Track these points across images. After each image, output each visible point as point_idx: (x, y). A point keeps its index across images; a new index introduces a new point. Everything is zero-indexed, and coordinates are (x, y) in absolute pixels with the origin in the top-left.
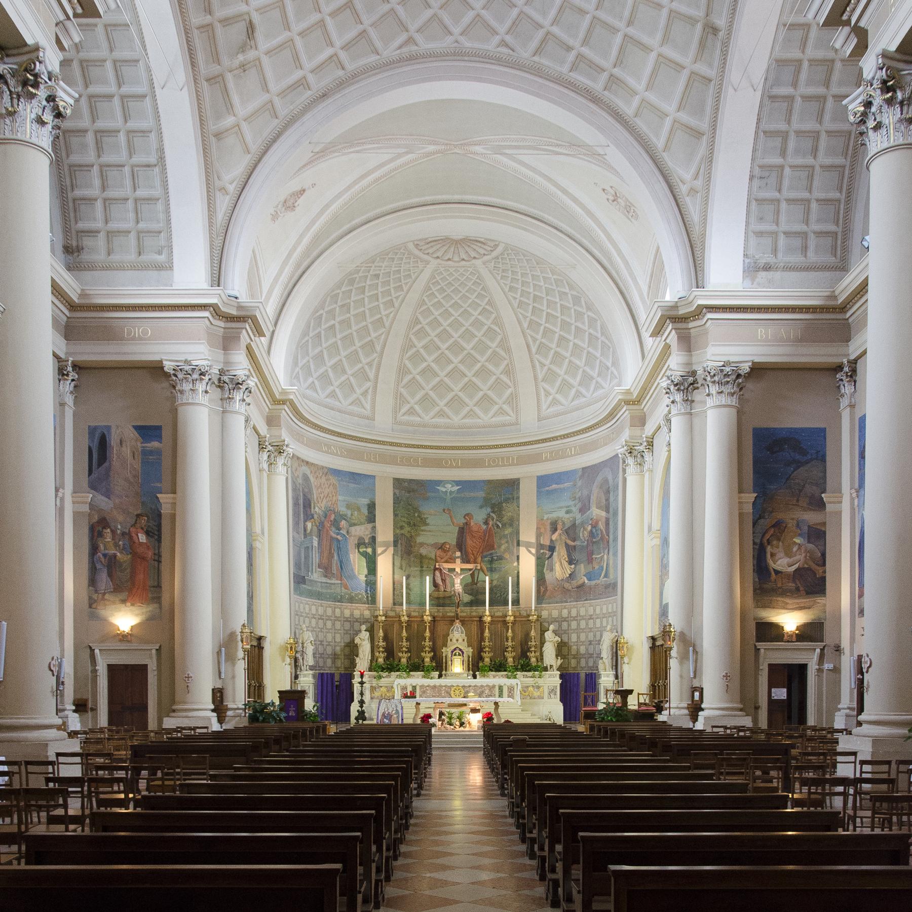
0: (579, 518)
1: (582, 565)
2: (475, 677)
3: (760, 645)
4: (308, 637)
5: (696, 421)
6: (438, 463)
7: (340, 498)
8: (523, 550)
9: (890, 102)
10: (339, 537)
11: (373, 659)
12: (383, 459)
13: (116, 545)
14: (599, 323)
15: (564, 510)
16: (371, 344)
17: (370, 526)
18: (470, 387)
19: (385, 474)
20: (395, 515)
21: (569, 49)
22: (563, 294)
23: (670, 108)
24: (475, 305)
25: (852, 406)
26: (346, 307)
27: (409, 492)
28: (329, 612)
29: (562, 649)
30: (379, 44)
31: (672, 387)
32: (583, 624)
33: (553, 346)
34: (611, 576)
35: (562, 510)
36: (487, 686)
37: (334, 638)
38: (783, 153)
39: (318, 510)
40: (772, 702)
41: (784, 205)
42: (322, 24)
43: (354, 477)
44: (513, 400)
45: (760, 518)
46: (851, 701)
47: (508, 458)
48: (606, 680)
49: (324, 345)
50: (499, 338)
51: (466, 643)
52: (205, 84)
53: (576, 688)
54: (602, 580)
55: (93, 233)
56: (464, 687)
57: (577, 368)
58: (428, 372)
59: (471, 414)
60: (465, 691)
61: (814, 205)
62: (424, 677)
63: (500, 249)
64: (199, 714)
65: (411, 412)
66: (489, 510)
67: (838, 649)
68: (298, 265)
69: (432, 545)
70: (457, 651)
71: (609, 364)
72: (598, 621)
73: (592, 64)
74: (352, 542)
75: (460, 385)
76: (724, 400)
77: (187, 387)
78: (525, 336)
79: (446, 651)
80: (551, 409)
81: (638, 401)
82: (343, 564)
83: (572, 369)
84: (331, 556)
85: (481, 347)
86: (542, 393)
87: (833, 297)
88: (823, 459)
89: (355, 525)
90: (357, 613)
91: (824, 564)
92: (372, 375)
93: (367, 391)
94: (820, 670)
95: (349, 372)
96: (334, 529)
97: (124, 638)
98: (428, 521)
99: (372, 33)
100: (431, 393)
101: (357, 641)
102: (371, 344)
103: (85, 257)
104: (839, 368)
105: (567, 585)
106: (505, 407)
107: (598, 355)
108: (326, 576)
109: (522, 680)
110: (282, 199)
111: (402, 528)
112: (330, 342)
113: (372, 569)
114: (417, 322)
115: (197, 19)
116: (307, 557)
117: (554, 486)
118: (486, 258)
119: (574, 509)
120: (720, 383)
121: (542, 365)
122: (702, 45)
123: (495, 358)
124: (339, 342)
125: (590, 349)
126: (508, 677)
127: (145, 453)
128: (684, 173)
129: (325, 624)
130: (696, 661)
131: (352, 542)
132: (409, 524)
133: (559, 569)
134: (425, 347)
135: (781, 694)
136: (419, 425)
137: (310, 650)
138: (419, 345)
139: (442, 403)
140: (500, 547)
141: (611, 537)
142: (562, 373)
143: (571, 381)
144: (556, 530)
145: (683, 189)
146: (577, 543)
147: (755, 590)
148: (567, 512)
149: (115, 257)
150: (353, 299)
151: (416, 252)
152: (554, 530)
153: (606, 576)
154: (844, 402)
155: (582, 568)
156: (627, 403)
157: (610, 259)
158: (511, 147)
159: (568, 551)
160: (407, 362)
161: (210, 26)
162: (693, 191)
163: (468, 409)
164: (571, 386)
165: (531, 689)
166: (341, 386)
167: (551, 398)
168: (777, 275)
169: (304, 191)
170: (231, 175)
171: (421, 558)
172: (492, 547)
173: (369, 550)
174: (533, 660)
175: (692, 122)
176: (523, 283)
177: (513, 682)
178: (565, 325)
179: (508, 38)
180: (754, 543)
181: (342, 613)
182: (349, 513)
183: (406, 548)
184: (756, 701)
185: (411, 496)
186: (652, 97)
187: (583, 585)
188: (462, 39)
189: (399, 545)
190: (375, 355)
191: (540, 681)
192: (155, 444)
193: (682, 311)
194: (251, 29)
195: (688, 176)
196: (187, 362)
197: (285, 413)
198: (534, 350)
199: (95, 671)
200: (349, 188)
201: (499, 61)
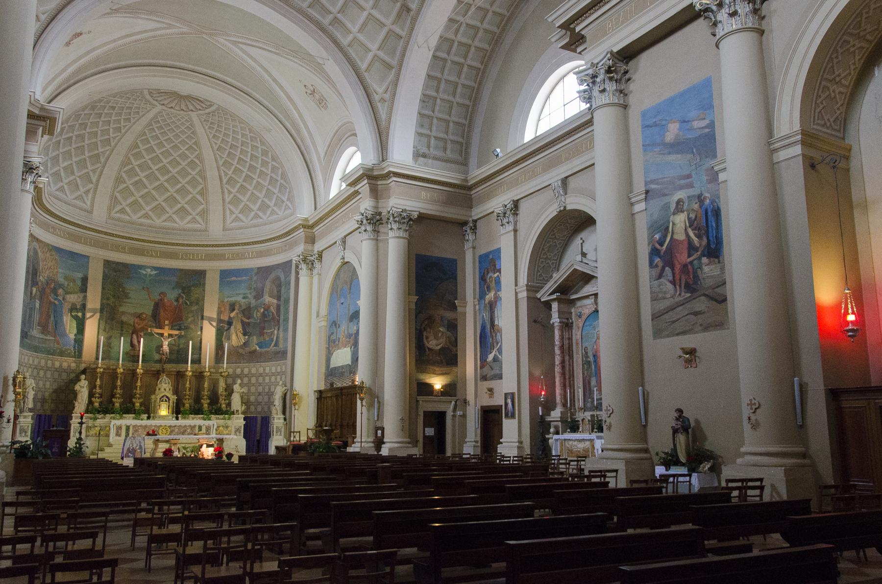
0: (253, 303)
1: (255, 337)
2: (177, 418)
3: (419, 398)
5: (381, 244)
6: (141, 252)
7: (60, 271)
8: (206, 324)
10: (56, 302)
11: (90, 402)
12: (97, 244)
14: (280, 171)
15: (241, 296)
16: (97, 156)
17: (82, 295)
18: (171, 200)
19: (98, 255)
20: (103, 288)
22: (254, 148)
23: (374, 47)
24: (183, 142)
25: (474, 248)
26: (84, 126)
27: (116, 272)
28: (43, 363)
31: (365, 221)
32: (253, 380)
33: (241, 180)
34: (281, 346)
35: (240, 296)
36: (190, 426)
37: (44, 385)
38: (437, 91)
39: (41, 278)
40: (425, 437)
41: (435, 121)
43: (72, 255)
44: (204, 213)
45: (420, 312)
46: (476, 436)
47: (198, 254)
48: (277, 421)
49: (61, 151)
50: (198, 169)
53: (256, 430)
54: (272, 348)
56: (170, 427)
57: (258, 198)
58: (139, 184)
59: (170, 219)
60: (171, 429)
61: (451, 124)
62: (135, 418)
63: (213, 109)
65: (122, 211)
66: (180, 291)
67: (465, 402)
68: (60, 86)
69: (132, 314)
71: (285, 199)
74: (66, 307)
76: (401, 233)
80: (233, 224)
81: (312, 227)
82: (58, 323)
83: (253, 198)
85: (183, 173)
86: (228, 212)
87: (466, 180)
88: (455, 278)
90: (65, 365)
91: (456, 346)
92: (94, 180)
93: (88, 191)
94: (454, 416)
95: (77, 174)
98: (130, 295)
100: (140, 200)
101: (77, 387)
102: (97, 156)
104: (465, 223)
105: (241, 351)
107: (276, 191)
108: (43, 333)
109: (215, 421)
111: (108, 299)
112: (66, 149)
113: (81, 330)
114: (137, 146)
116: (30, 316)
117: (234, 278)
118: (200, 112)
119: (249, 296)
120: (399, 222)
121: (230, 192)
122: (399, 16)
123: (193, 182)
124: (73, 150)
125: (270, 187)
128: (378, 89)
129: (38, 373)
130: (379, 409)
132: (114, 296)
133: (236, 338)
135: (430, 432)
136: (129, 222)
137: (31, 395)
139: (148, 208)
140: (187, 319)
141: (282, 317)
143: (252, 207)
144: (234, 310)
145: (377, 98)
146: (251, 320)
147: (416, 360)
148: (244, 298)
150: (91, 120)
151: (148, 97)
153: (276, 345)
154: (468, 246)
155: (255, 339)
156: (304, 226)
157: (298, 131)
159: (243, 325)
160: (124, 175)
162: (382, 100)
163: (168, 215)
164: (251, 210)
165: (221, 428)
166: (69, 183)
167: (234, 216)
168: (430, 161)
169: (81, 34)
171: (122, 323)
172: (181, 319)
173: (80, 314)
174: (224, 406)
175: (387, 59)
176: (225, 134)
177: (207, 423)
178: (252, 168)
180: (416, 329)
181: (53, 364)
182: (66, 283)
183: (110, 315)
184: (416, 437)
185: (117, 276)
186: (361, 37)
187: (255, 351)
190: (99, 165)
191: (229, 422)
193: (375, 173)
195: (380, 90)
198: (225, 181)
200: (115, 41)
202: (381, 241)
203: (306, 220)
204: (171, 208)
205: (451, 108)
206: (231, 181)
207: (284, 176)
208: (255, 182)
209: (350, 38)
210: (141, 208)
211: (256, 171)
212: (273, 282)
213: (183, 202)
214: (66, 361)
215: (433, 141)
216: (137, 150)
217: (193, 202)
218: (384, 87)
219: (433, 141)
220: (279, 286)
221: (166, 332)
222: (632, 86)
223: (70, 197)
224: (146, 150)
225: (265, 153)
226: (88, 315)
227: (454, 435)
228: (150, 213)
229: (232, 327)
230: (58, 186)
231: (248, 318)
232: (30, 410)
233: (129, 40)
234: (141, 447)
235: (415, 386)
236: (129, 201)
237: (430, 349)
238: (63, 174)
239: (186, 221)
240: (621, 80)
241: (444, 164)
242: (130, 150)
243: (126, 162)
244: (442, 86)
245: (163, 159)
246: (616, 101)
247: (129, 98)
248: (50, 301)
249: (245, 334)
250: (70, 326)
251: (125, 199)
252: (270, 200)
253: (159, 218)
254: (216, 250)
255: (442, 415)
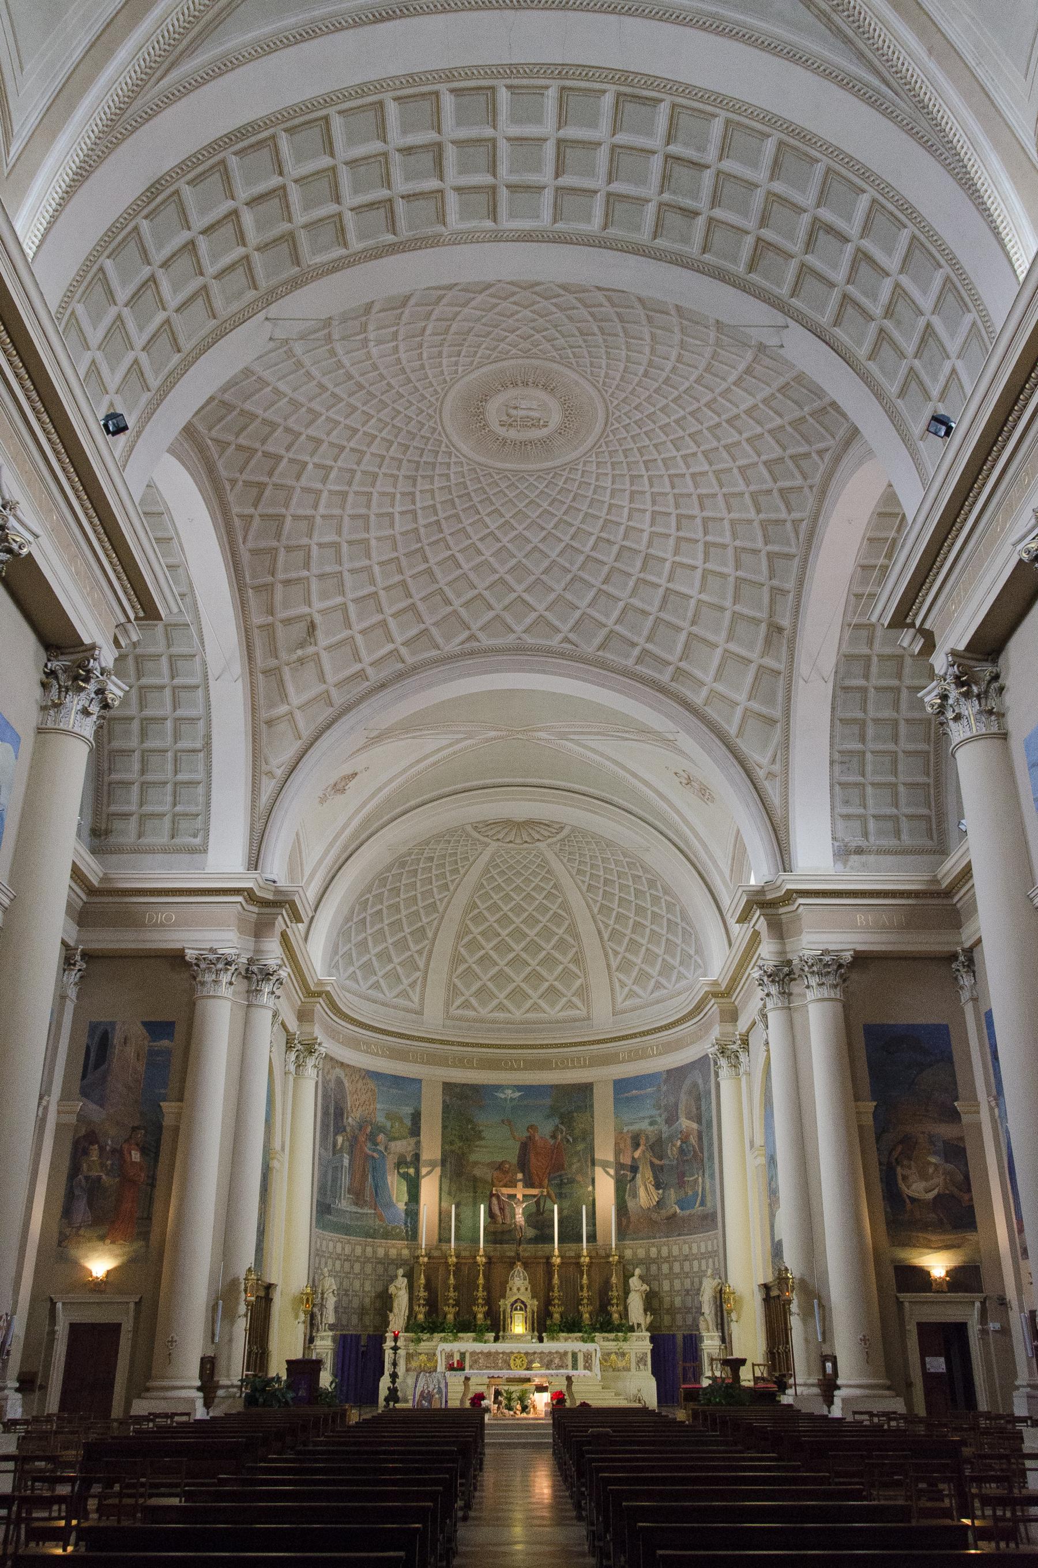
1: (672, 1191)
2: (541, 1340)
4: (330, 1284)
5: (796, 1016)
7: (378, 1106)
8: (599, 1171)
9: (967, 695)
10: (375, 1155)
12: (432, 1060)
13: (103, 1165)
14: (678, 908)
15: (647, 1121)
18: (535, 977)
19: (434, 1076)
20: (444, 1127)
21: (634, 645)
23: (741, 697)
26: (396, 891)
28: (358, 1250)
29: (651, 1302)
30: (440, 641)
31: (765, 979)
32: (677, 1268)
33: (628, 932)
34: (709, 1204)
35: (645, 1121)
38: (863, 739)
39: (351, 1121)
40: (927, 1376)
41: (869, 790)
42: (384, 623)
43: (397, 1081)
44: (583, 992)
48: (710, 1344)
51: (529, 1294)
52: (261, 676)
54: (698, 1209)
55: (126, 816)
56: (527, 1354)
58: (485, 961)
59: (535, 1007)
61: (901, 789)
62: (475, 1340)
64: (183, 1395)
65: (466, 1005)
66: (557, 1121)
67: (1003, 1302)
70: (519, 1304)
71: (692, 952)
72: (696, 1263)
73: (657, 658)
74: (391, 1160)
75: (523, 976)
76: (825, 992)
77: (209, 978)
78: (595, 921)
79: (505, 1304)
80: (627, 1003)
81: (728, 993)
82: (379, 1188)
83: (650, 957)
84: (364, 1176)
85: (547, 933)
86: (617, 984)
87: (935, 881)
89: (395, 1139)
92: (421, 964)
93: (415, 982)
94: (984, 1332)
95: (396, 960)
96: (369, 1144)
97: (98, 1287)
98: (484, 1134)
99: (434, 631)
100: (490, 984)
101: (392, 1289)
103: (112, 840)
104: (953, 957)
105: (654, 1216)
106: (574, 999)
108: (356, 1204)
109: (600, 1345)
110: (332, 782)
111: (451, 1143)
114: (475, 906)
115: (258, 619)
116: (335, 1180)
118: (550, 840)
119: (659, 1119)
120: (819, 974)
121: (616, 953)
122: (768, 642)
126: (584, 1341)
127: (152, 1053)
128: (760, 758)
129: (352, 1267)
131: (391, 1160)
132: (461, 1138)
133: (645, 1196)
134: (483, 934)
136: (475, 1021)
137: (331, 1302)
138: (476, 930)
139: (502, 996)
140: (570, 1166)
141: (706, 1154)
142: (639, 961)
145: (761, 773)
148: (651, 1124)
149: (144, 840)
152: (636, 1145)
153: (703, 1203)
154: (965, 995)
156: (715, 995)
157: (687, 842)
158: (575, 733)
161: (271, 625)
164: (649, 976)
165: (613, 1357)
167: (627, 989)
168: (872, 859)
170: (279, 759)
171: (475, 1179)
172: (560, 1167)
173: (412, 1171)
175: (764, 710)
176: (592, 866)
177: (589, 1347)
178: (640, 910)
179: (571, 636)
181: (374, 1252)
182: (389, 1124)
183: (458, 1172)
185: (463, 1104)
186: (720, 687)
187: (675, 1215)
188: (524, 636)
189: (448, 1165)
191: (625, 1346)
192: (165, 1043)
193: (769, 897)
194: (312, 627)
195: (764, 761)
196: (212, 950)
197: (320, 1007)
198: (606, 936)
199: (52, 1333)
200: (405, 771)
201: (562, 655)
202: (796, 1009)
203: (715, 983)
204: (535, 989)
205: (895, 762)
206: (615, 935)
207: (684, 917)
208: (648, 930)
209: (704, 692)
210: (492, 996)
211: (642, 915)
212: (690, 1093)
213: (551, 977)
214: (393, 1246)
215: (872, 825)
216: (476, 911)
217: (567, 976)
218: (769, 754)
219: (872, 825)
220: (698, 1099)
221: (520, 1191)
222: (1009, 698)
223: (389, 995)
224: (488, 909)
225: (652, 883)
226: (424, 1171)
227: (989, 1370)
228: (505, 1001)
229: (639, 1176)
230: (370, 983)
231: (661, 1158)
232: (332, 1327)
233: (422, 765)
234: (440, 1391)
235: (892, 1272)
236: (474, 988)
237: (913, 1200)
238: (376, 964)
239: (558, 1007)
240: (986, 692)
241: (890, 858)
242: (466, 913)
243: (463, 932)
244: (870, 732)
245: (515, 919)
246: (984, 731)
247: (449, 842)
248: (367, 1156)
249: (658, 1186)
250: (397, 1190)
251: (468, 987)
252: (673, 956)
253: (519, 1007)
254: (604, 1048)
255: (960, 1329)
